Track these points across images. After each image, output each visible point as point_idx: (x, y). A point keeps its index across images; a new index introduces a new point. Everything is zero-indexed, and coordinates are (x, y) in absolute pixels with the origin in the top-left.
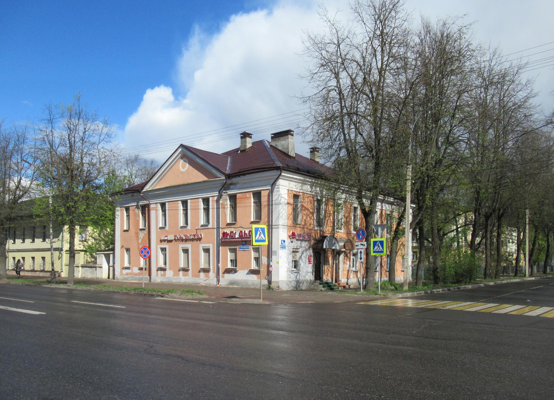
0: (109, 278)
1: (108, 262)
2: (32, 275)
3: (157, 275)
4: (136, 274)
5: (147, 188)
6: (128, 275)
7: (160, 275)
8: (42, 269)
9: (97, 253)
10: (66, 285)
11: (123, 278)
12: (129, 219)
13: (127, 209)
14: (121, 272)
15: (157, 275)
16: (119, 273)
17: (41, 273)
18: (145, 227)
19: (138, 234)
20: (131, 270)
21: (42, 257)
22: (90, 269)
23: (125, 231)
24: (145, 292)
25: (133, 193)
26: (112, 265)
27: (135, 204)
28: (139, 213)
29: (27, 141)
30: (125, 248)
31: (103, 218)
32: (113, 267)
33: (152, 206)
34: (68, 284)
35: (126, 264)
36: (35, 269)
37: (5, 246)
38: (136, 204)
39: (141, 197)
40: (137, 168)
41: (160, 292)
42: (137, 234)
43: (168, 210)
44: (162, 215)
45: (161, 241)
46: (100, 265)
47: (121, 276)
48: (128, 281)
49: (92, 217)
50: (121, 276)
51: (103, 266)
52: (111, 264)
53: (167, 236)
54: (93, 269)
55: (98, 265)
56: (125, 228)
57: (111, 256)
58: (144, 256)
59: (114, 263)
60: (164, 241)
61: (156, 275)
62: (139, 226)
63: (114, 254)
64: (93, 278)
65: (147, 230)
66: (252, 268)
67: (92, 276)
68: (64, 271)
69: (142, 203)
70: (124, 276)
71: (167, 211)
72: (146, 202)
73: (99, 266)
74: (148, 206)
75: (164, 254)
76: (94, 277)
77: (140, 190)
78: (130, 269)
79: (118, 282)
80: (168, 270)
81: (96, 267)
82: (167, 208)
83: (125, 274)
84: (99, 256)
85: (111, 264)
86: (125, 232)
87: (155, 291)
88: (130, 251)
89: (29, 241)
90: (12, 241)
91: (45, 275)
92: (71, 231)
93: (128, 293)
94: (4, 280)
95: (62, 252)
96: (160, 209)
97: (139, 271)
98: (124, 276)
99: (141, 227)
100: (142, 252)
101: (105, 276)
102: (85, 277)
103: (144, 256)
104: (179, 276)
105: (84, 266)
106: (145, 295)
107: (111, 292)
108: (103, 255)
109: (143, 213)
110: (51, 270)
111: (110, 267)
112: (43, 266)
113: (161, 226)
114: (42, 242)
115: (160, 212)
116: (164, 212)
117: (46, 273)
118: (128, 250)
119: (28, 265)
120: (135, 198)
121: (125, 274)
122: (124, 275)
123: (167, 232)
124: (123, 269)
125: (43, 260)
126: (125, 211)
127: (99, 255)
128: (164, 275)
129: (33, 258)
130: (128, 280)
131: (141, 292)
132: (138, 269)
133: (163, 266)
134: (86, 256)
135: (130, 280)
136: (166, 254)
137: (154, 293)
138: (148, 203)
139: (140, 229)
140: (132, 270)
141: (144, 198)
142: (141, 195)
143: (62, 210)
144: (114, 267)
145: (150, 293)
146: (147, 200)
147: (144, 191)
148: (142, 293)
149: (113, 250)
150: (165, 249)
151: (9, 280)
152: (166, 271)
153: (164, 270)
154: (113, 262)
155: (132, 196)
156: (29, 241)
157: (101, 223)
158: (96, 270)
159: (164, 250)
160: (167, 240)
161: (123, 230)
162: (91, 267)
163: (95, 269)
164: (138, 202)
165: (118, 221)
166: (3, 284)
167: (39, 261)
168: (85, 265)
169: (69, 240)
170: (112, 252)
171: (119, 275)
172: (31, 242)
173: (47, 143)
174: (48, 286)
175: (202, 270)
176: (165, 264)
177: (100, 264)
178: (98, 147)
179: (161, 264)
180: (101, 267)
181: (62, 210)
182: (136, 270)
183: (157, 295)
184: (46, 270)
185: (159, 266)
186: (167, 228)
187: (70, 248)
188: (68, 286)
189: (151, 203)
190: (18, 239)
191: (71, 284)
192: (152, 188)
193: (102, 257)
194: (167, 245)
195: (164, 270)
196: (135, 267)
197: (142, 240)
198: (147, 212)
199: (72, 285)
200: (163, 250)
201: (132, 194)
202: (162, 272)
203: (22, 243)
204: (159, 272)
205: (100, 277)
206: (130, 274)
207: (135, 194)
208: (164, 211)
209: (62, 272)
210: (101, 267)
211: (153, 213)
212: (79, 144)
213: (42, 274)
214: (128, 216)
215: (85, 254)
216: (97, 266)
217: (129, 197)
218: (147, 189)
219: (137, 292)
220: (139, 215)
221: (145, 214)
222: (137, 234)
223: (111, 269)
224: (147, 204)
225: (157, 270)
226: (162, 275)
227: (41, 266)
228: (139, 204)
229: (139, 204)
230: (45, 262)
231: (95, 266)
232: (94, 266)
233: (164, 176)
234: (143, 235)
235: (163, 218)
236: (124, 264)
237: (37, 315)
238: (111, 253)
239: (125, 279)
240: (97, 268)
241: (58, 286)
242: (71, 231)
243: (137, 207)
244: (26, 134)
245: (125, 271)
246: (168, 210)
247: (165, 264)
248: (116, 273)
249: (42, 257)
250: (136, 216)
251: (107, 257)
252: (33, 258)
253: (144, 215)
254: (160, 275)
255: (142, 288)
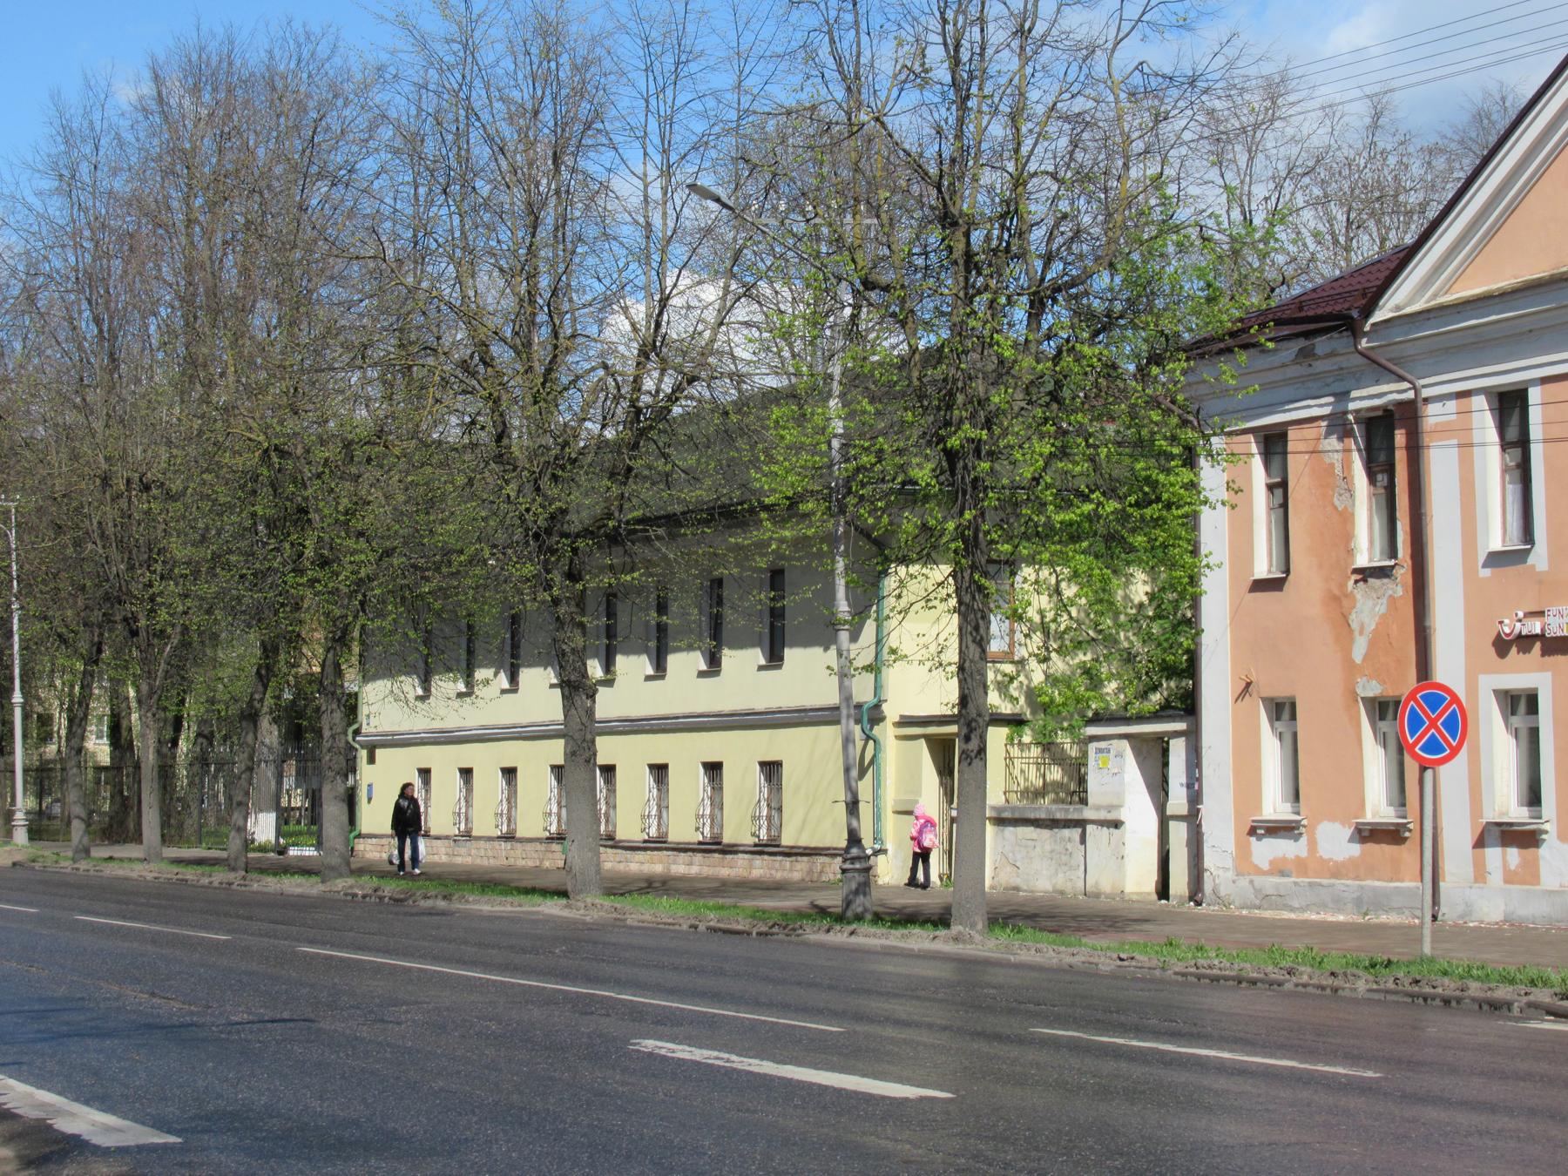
0: (1163, 891)
1: (1159, 787)
2: (707, 871)
3: (1480, 874)
4: (1337, 871)
5: (1401, 298)
6: (1282, 873)
7: (1496, 878)
8: (653, 832)
9: (1092, 730)
10: (942, 932)
11: (1257, 891)
12: (1285, 506)
13: (1273, 443)
14: (1243, 853)
15: (1480, 874)
16: (1229, 863)
17: (758, 861)
18: (1392, 552)
19: (1345, 603)
20: (1304, 840)
21: (763, 764)
22: (1045, 833)
23: (1260, 586)
24: (1448, 986)
25: (1307, 335)
26: (1184, 811)
27: (1320, 407)
28: (1347, 465)
29: (693, 67)
30: (1264, 699)
31: (1150, 512)
32: (1192, 818)
33: (1434, 416)
34: (956, 929)
35: (1274, 806)
36: (727, 838)
37: (589, 703)
38: (1327, 410)
39: (1359, 360)
40: (1282, 166)
41: (1546, 983)
42: (1338, 605)
43: (1545, 441)
44: (1505, 470)
45: (1502, 646)
46: (1110, 808)
47: (1243, 882)
48: (1293, 916)
49: (1088, 508)
50: (1243, 882)
51: (1123, 815)
52: (1178, 801)
53: (1541, 614)
54: (1066, 832)
55: (1098, 808)
56: (1263, 568)
57: (1178, 749)
58: (1424, 749)
59: (1195, 798)
60: (1525, 642)
61: (1469, 870)
62: (1350, 553)
63: (1193, 737)
64: (1062, 893)
65: (1404, 573)
66: (1369, 817)
67: (1061, 881)
68: (889, 846)
69: (1369, 397)
70: (1260, 881)
71: (1537, 452)
72: (1390, 392)
73: (1103, 815)
74: (1407, 414)
75: (1524, 735)
76: (1068, 888)
77: (1355, 314)
78: (1297, 838)
79: (1231, 924)
80: (1551, 838)
81: (1081, 824)
82: (1536, 432)
83: (1265, 866)
84: (1100, 751)
85: (1178, 801)
86: (1259, 595)
87: (1512, 981)
88: (1293, 717)
89: (742, 662)
90: (644, 665)
91: (779, 875)
92: (967, 598)
93: (1335, 990)
94: (589, 900)
95: (877, 731)
96: (1492, 435)
97: (1356, 849)
98: (1260, 881)
99: (1362, 561)
100: (1451, 724)
101: (1139, 879)
102: (1017, 889)
103: (1424, 749)
104: (1538, 883)
105: (1006, 815)
106: (1447, 1002)
107: (1226, 978)
108: (1125, 745)
109: (1379, 465)
110: (844, 844)
111: (1172, 824)
112: (660, 817)
113: (1496, 545)
114: (761, 668)
115: (1491, 459)
116: (1517, 452)
117: (787, 862)
118: (1282, 710)
119: (438, 816)
120: (1319, 366)
121: (1265, 866)
122: (1259, 871)
123: (1540, 580)
124: (1252, 831)
125: (769, 779)
126: (1257, 463)
127: (1103, 745)
128: (1529, 875)
129: (714, 769)
130: (1292, 910)
131: (1417, 982)
132: (1348, 832)
133: (1516, 813)
134: (1015, 751)
135: (1302, 909)
136: (1534, 733)
137: (1503, 992)
138: (1411, 395)
139: (1356, 571)
140: (1312, 844)
141: (1380, 368)
142: (1364, 343)
143: (923, 473)
144: (1199, 826)
145: (1475, 989)
146: (1402, 379)
147: (1379, 316)
148: (1428, 990)
149: (1188, 706)
150: (1531, 701)
151: (619, 902)
152: (1543, 851)
153: (1523, 838)
154: (1189, 786)
155: (1306, 355)
156: (742, 662)
157: (1139, 540)
158: (1083, 841)
159: (1522, 707)
160: (1540, 637)
161: (1248, 584)
162: (1053, 824)
163: (1075, 833)
164: (1343, 396)
165: (1214, 529)
166: (584, 923)
167: (743, 782)
168: (1014, 809)
169: (952, 655)
170: (1181, 726)
171: (1230, 875)
172: (701, 674)
173: (832, 75)
174: (838, 936)
175: (1496, 831)
176: (1533, 797)
177: (1105, 801)
178: (1114, 62)
179: (1507, 804)
180: (1117, 824)
181: (923, 473)
182: (1335, 842)
183: (1530, 1005)
184: (787, 840)
185: (1491, 815)
186: (1540, 557)
187: (964, 701)
188: (956, 939)
189: (1425, 393)
190: (628, 652)
191: (973, 926)
192: (1435, 296)
193: (1120, 755)
194: (1542, 669)
195: (1523, 838)
196: (1332, 819)
197: (1373, 644)
198: (1401, 457)
199: (977, 937)
200: (1521, 704)
201: (1302, 343)
202: (1513, 853)
203: (648, 678)
204: (1493, 854)
205: (1106, 886)
206: (1301, 866)
207: (1322, 344)
208: (1517, 443)
209: (882, 851)
210: (1117, 824)
211: (1441, 464)
212: (1005, 63)
213: (760, 868)
214: (1279, 487)
215: (1010, 740)
216: (1088, 814)
217: (1284, 365)
218: (1398, 308)
219: (1391, 985)
220: (1347, 479)
221: (1390, 470)
222: (1338, 605)
223: (1179, 832)
224: (1400, 404)
225: (1480, 843)
226: (1510, 877)
227: (756, 818)
228: (1352, 406)
229: (1352, 406)
230: (780, 789)
231: (1075, 816)
232: (1073, 813)
233: (1511, 210)
234: (1381, 608)
235: (1513, 491)
236: (1258, 807)
237: (906, 1100)
238: (1177, 734)
239: (1265, 899)
240: (1090, 828)
241: (896, 938)
242: (967, 598)
243: (1338, 425)
244: (690, 28)
245: (1266, 850)
246: (1545, 441)
247: (1533, 797)
248: (1208, 862)
249: (763, 764)
250: (1333, 483)
251: (1153, 755)
252: (714, 769)
253: (1382, 478)
254: (1496, 878)
255: (1422, 960)
